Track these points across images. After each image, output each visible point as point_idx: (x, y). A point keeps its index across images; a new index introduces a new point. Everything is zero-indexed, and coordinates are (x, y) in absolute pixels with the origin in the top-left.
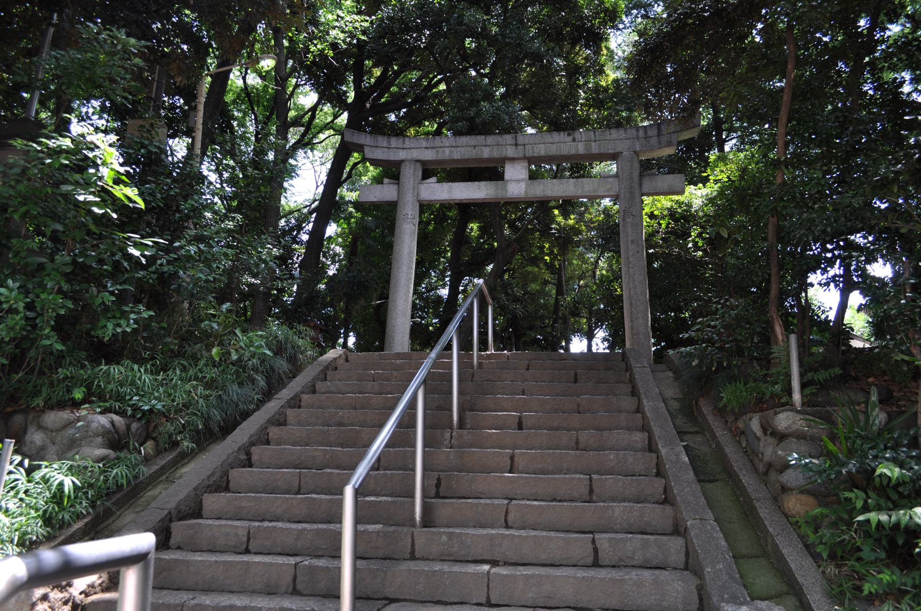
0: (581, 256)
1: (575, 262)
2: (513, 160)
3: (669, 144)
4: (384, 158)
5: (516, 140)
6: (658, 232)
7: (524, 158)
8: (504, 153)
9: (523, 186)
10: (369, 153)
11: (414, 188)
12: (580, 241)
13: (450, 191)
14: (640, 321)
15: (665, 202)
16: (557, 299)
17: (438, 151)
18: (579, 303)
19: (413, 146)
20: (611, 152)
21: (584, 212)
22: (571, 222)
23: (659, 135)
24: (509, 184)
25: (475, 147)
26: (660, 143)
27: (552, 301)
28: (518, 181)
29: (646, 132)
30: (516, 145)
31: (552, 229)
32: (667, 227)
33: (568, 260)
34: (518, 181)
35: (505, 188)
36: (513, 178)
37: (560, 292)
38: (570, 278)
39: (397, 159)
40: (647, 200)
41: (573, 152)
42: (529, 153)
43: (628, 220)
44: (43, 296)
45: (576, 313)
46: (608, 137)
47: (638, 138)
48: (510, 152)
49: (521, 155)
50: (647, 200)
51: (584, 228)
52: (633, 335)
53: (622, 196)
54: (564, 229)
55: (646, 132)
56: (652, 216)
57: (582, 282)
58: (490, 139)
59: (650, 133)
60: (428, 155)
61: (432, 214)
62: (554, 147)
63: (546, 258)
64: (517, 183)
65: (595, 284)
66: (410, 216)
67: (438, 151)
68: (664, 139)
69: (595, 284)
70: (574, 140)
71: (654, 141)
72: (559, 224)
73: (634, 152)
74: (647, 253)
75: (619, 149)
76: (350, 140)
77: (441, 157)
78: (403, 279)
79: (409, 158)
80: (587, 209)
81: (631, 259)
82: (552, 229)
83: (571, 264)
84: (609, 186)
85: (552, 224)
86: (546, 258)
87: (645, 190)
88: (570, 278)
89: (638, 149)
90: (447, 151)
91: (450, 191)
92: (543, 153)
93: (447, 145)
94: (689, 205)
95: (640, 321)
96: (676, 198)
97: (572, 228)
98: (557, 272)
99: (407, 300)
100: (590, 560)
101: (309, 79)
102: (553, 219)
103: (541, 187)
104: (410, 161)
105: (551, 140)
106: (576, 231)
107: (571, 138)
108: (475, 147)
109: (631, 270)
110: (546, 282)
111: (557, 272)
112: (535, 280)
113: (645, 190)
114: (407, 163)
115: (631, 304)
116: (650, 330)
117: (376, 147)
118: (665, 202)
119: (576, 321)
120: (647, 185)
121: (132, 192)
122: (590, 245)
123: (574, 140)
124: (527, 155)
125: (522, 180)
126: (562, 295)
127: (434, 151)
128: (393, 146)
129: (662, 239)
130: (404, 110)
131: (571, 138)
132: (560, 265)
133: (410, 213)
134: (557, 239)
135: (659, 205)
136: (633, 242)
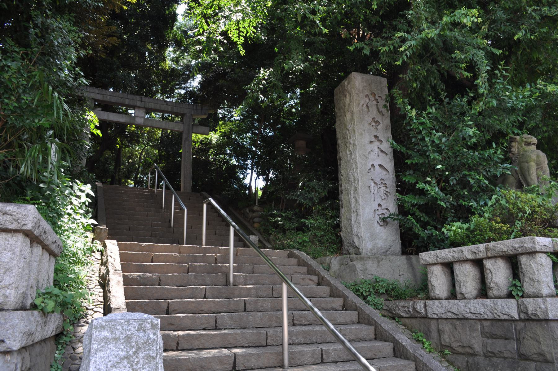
3: (205, 114)
7: (144, 108)
15: (201, 137)
23: (202, 110)
25: (122, 98)
30: (141, 101)
40: (194, 135)
42: (147, 106)
44: (123, 347)
49: (143, 106)
50: (194, 135)
60: (99, 97)
62: (158, 106)
75: (185, 112)
90: (108, 97)
92: (153, 107)
94: (211, 141)
96: (205, 136)
100: (373, 336)
101: (16, 44)
108: (122, 98)
113: (194, 131)
118: (201, 137)
120: (195, 129)
121: (99, 132)
130: (397, 63)
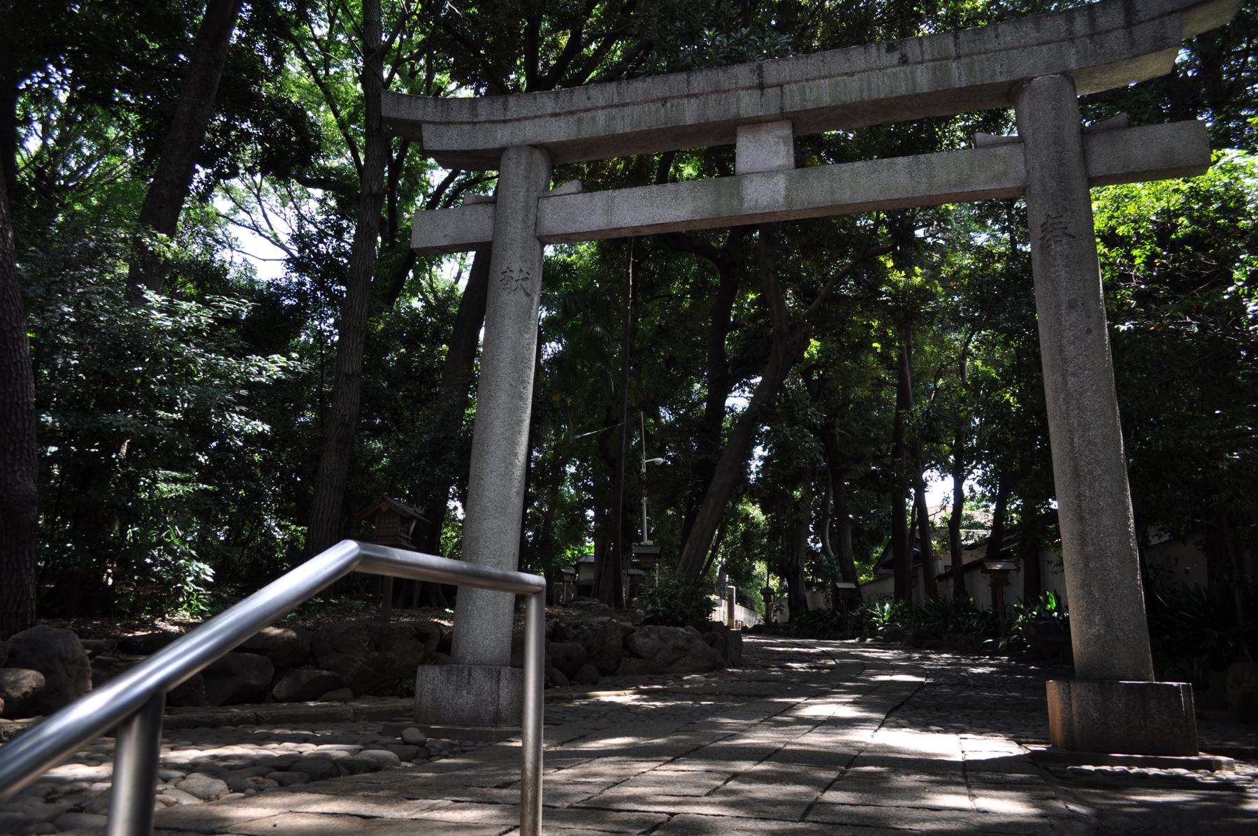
0: (938, 340)
1: (927, 348)
2: (755, 123)
4: (464, 148)
5: (760, 76)
6: (1126, 278)
8: (733, 109)
9: (781, 183)
10: (431, 142)
11: (527, 208)
12: (932, 314)
13: (609, 210)
14: (1106, 520)
15: (1149, 198)
16: (898, 414)
17: (580, 121)
18: (936, 420)
19: (524, 113)
20: (1000, 79)
21: (941, 263)
22: (917, 280)
23: (1129, 24)
24: (746, 182)
25: (664, 101)
26: (1132, 44)
27: (892, 415)
28: (769, 173)
29: (1092, 21)
30: (761, 87)
31: (881, 294)
32: (1149, 262)
33: (915, 346)
34: (769, 173)
35: (737, 194)
36: (758, 167)
37: (904, 402)
38: (922, 374)
39: (490, 146)
41: (903, 90)
42: (793, 103)
43: (1056, 249)
45: (933, 436)
46: (994, 45)
47: (1071, 38)
48: (748, 104)
49: (774, 110)
51: (940, 289)
52: (1086, 559)
53: (1036, 188)
54: (905, 292)
55: (1092, 21)
56: (1111, 239)
57: (941, 382)
58: (700, 81)
59: (1103, 21)
60: (559, 131)
61: (686, 281)
63: (875, 345)
64: (767, 177)
65: (965, 385)
66: (515, 275)
67: (580, 121)
68: (1144, 33)
69: (965, 385)
70: (904, 61)
71: (1117, 41)
72: (894, 285)
73: (1064, 74)
74: (1114, 334)
75: (1020, 72)
76: (393, 115)
77: (587, 132)
78: (497, 423)
79: (516, 141)
80: (944, 255)
81: (1070, 351)
82: (881, 294)
83: (920, 351)
84: (999, 167)
85: (881, 285)
86: (875, 345)
87: (1097, 168)
88: (922, 374)
89: (1073, 65)
90: (601, 116)
91: (609, 210)
92: (826, 100)
93: (601, 103)
95: (1106, 520)
97: (919, 290)
98: (899, 369)
99: (508, 474)
102: (881, 274)
103: (827, 184)
104: (518, 148)
105: (846, 67)
106: (923, 294)
107: (896, 56)
108: (664, 101)
109: (1071, 380)
110: (881, 383)
111: (899, 369)
112: (860, 382)
114: (511, 153)
115: (1076, 473)
116: (1133, 544)
117: (447, 123)
118: (1149, 198)
119: (932, 449)
122: (957, 321)
123: (904, 61)
124: (788, 108)
125: (778, 171)
126: (908, 407)
127: (571, 119)
128: (482, 118)
129: (1138, 295)
131: (896, 56)
132: (900, 357)
133: (516, 267)
134: (892, 311)
135: (1131, 209)
136: (1072, 305)
